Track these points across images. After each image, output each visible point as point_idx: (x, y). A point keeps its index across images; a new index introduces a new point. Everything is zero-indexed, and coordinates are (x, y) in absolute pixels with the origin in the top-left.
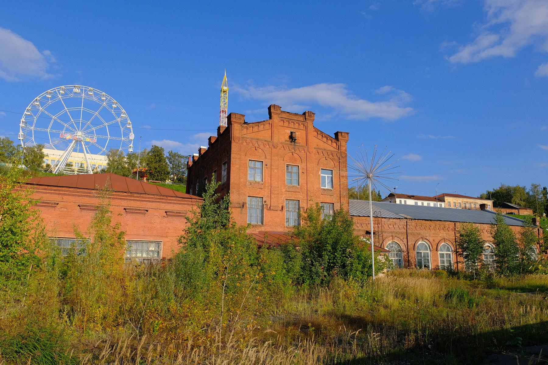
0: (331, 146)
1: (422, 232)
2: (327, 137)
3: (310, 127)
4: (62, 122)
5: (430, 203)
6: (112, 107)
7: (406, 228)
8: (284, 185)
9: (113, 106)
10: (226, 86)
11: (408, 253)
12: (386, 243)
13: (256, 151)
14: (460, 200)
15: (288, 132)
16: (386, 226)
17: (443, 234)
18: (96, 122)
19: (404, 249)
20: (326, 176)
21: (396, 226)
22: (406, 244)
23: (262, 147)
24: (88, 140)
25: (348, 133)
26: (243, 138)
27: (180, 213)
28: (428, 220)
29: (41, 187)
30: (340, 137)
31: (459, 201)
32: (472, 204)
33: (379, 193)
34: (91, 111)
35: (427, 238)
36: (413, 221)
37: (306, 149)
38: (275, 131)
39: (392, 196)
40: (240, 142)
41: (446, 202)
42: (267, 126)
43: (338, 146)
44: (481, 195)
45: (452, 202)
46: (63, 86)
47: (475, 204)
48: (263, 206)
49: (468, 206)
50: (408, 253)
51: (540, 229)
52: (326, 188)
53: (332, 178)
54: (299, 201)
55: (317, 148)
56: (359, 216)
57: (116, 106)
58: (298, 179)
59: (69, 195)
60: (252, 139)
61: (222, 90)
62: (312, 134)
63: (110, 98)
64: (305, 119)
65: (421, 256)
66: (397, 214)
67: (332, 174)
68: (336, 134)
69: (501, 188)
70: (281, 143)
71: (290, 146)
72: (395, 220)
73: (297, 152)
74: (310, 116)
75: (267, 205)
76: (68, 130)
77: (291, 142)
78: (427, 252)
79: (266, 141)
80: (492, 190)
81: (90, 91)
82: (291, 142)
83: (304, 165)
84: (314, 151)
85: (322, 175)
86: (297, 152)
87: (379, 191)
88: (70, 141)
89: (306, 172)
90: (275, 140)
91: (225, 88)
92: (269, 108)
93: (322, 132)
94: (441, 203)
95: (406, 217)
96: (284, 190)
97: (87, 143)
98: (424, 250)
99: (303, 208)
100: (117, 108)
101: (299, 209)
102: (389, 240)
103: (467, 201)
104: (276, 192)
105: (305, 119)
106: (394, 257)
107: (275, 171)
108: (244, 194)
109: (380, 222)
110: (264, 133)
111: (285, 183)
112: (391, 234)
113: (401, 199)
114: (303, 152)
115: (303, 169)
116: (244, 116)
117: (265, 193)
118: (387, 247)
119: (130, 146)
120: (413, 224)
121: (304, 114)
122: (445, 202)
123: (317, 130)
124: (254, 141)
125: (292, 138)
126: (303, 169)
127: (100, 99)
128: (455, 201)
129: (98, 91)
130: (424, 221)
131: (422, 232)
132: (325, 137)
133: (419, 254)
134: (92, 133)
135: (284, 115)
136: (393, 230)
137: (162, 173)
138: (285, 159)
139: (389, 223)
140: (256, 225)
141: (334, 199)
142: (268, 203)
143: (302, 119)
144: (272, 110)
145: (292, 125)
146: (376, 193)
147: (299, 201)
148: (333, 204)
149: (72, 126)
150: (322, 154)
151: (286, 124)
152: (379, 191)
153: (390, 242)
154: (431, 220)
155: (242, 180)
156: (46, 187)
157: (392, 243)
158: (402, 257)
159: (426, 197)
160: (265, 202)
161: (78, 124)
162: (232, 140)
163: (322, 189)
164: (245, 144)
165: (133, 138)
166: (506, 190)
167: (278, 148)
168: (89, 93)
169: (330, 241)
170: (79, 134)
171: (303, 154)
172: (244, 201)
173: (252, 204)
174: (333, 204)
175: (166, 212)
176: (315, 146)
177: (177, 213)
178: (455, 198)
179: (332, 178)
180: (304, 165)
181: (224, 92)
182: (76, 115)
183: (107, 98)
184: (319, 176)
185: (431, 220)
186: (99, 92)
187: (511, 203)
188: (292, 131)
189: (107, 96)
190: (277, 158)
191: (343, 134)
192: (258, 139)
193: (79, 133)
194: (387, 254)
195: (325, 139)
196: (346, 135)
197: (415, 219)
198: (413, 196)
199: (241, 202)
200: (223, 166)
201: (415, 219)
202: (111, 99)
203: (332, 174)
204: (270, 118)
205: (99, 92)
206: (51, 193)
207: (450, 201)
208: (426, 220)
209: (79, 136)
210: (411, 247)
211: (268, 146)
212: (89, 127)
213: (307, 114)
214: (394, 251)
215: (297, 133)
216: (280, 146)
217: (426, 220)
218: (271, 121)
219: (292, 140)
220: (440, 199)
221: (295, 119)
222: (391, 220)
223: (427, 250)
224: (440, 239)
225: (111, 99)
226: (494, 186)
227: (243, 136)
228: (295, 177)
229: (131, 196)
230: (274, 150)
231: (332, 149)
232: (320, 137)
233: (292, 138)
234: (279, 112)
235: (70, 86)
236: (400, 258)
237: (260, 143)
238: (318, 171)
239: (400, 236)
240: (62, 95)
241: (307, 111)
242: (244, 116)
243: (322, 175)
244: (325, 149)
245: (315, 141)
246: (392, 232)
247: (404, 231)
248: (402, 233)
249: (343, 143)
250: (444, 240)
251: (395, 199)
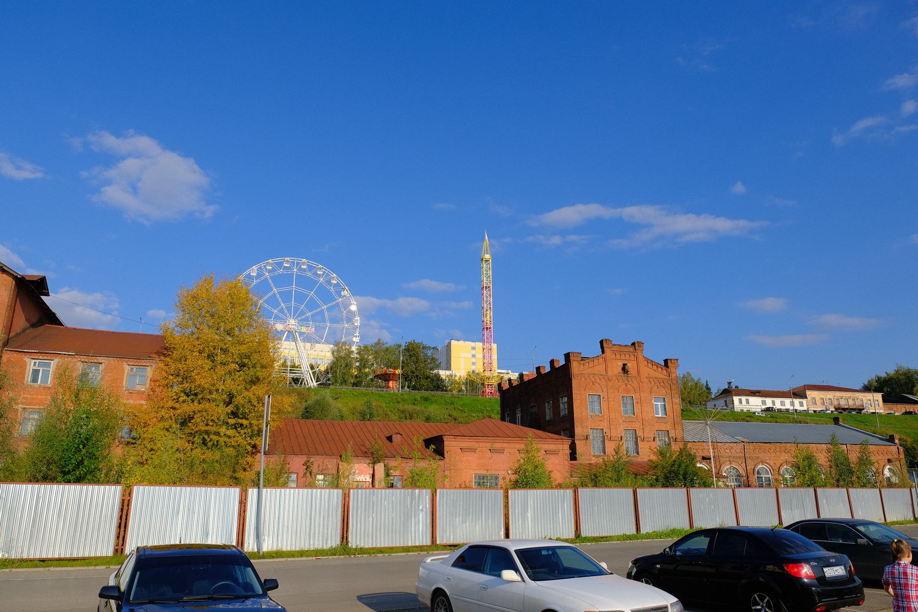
0: (661, 374)
1: (761, 455)
2: (657, 365)
3: (640, 357)
4: (270, 308)
5: (784, 401)
6: (331, 284)
7: (743, 452)
8: (621, 416)
9: (332, 282)
10: (487, 254)
11: (748, 478)
12: (724, 468)
13: (594, 386)
14: (830, 395)
15: (621, 364)
16: (722, 451)
17: (784, 457)
18: (312, 305)
19: (744, 474)
20: (659, 403)
21: (733, 451)
22: (745, 469)
23: (598, 381)
24: (304, 329)
25: (677, 360)
26: (581, 374)
27: (555, 451)
28: (767, 443)
29: (466, 437)
30: (670, 364)
31: (829, 396)
32: (849, 400)
33: (707, 385)
34: (320, 302)
35: (768, 462)
36: (751, 445)
37: (638, 380)
38: (609, 365)
39: (727, 393)
40: (579, 378)
41: (809, 398)
42: (601, 360)
43: (668, 373)
44: (869, 382)
45: (817, 399)
46: (271, 260)
47: (853, 400)
48: (604, 437)
49: (843, 403)
50: (748, 478)
51: (900, 447)
52: (660, 416)
53: (665, 405)
54: (636, 430)
55: (649, 377)
56: (694, 442)
57: (336, 282)
58: (632, 409)
59: (482, 442)
60: (589, 374)
61: (484, 259)
62: (643, 363)
63: (329, 272)
64: (635, 349)
65: (762, 481)
66: (733, 437)
67: (664, 402)
68: (666, 361)
69: (897, 372)
70: (615, 375)
71: (623, 378)
72: (731, 444)
73: (630, 383)
74: (639, 346)
75: (607, 436)
76: (277, 318)
77: (624, 374)
78: (768, 476)
79: (601, 375)
80: (883, 375)
81: (304, 263)
82: (624, 374)
83: (638, 395)
84: (646, 380)
85: (655, 403)
86: (630, 383)
87: (707, 382)
88: (282, 332)
89: (641, 402)
90: (610, 374)
91: (487, 256)
92: (601, 342)
93: (652, 361)
94: (801, 400)
95: (743, 440)
96: (622, 421)
97: (301, 334)
98: (765, 474)
99: (640, 437)
100: (337, 285)
101: (636, 438)
102: (726, 465)
103: (841, 395)
104: (615, 423)
105: (635, 349)
106: (733, 482)
107: (612, 403)
108: (587, 427)
109: (716, 447)
110: (600, 368)
111: (621, 415)
112: (728, 459)
113: (740, 397)
114: (636, 382)
115: (637, 399)
116: (581, 353)
117: (604, 425)
118: (725, 472)
119: (355, 335)
120: (751, 447)
121: (633, 344)
122: (807, 398)
123: (647, 360)
124: (591, 377)
125: (624, 369)
126: (637, 399)
127: (316, 274)
128: (822, 396)
129: (313, 264)
130: (763, 444)
131: (761, 455)
132: (655, 365)
133: (761, 479)
134: (307, 319)
135: (615, 348)
136: (730, 454)
137: (420, 378)
138: (620, 391)
139: (725, 447)
140: (599, 456)
141: (668, 427)
142: (608, 434)
143: (632, 349)
144: (605, 345)
145: (623, 357)
146: (703, 385)
147: (636, 430)
148: (668, 431)
149: (282, 311)
150: (653, 383)
151: (618, 356)
152: (707, 382)
153: (728, 467)
154: (770, 443)
155: (584, 414)
156: (470, 437)
157: (730, 468)
158: (741, 483)
159: (779, 391)
160: (606, 433)
161: (289, 309)
162: (572, 377)
163: (656, 417)
164: (583, 380)
165: (359, 324)
166: (905, 374)
167: (613, 381)
168: (302, 267)
169: (681, 473)
170: (292, 323)
171: (636, 385)
172: (587, 434)
173: (595, 436)
174: (668, 431)
175: (545, 451)
176: (646, 375)
177: (553, 451)
178: (823, 392)
179: (665, 405)
180: (638, 395)
181: (486, 261)
182: (286, 296)
183: (324, 272)
184: (653, 404)
185: (770, 443)
186: (342, 283)
187: (912, 394)
188: (624, 363)
189: (324, 269)
190: (612, 390)
191: (673, 362)
192: (594, 374)
193: (292, 321)
194: (725, 480)
195: (655, 367)
196: (676, 361)
197: (752, 442)
198: (759, 392)
199: (585, 435)
200: (546, 403)
201: (752, 442)
202: (298, 260)
203: (664, 402)
204: (603, 352)
205: (342, 283)
206: (472, 442)
207: (814, 396)
208: (764, 443)
209: (292, 325)
210: (750, 471)
211: (603, 380)
212: (303, 313)
213: (636, 345)
214: (733, 476)
215: (628, 365)
216: (614, 378)
217: (764, 443)
218: (604, 356)
219: (625, 371)
220: (799, 394)
221: (626, 350)
222: (727, 444)
223: (769, 474)
224: (781, 462)
225: (298, 260)
226: (886, 369)
227: (582, 372)
228: (629, 407)
229: (521, 440)
230: (610, 384)
231: (662, 376)
232: (650, 365)
233: (624, 369)
234: (610, 346)
235: (279, 260)
236: (740, 484)
237: (596, 378)
238: (651, 400)
239: (738, 460)
240: (270, 271)
241: (636, 342)
242: (581, 353)
243: (655, 403)
244: (656, 378)
245: (646, 370)
246: (729, 457)
247: (742, 455)
248: (740, 457)
249: (673, 370)
250: (787, 462)
251: (733, 398)
